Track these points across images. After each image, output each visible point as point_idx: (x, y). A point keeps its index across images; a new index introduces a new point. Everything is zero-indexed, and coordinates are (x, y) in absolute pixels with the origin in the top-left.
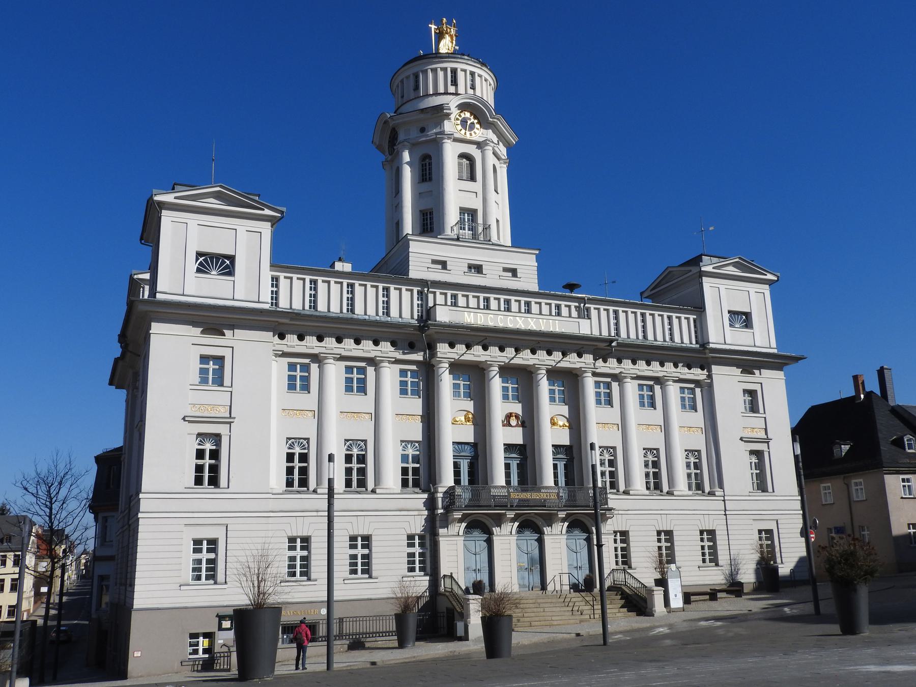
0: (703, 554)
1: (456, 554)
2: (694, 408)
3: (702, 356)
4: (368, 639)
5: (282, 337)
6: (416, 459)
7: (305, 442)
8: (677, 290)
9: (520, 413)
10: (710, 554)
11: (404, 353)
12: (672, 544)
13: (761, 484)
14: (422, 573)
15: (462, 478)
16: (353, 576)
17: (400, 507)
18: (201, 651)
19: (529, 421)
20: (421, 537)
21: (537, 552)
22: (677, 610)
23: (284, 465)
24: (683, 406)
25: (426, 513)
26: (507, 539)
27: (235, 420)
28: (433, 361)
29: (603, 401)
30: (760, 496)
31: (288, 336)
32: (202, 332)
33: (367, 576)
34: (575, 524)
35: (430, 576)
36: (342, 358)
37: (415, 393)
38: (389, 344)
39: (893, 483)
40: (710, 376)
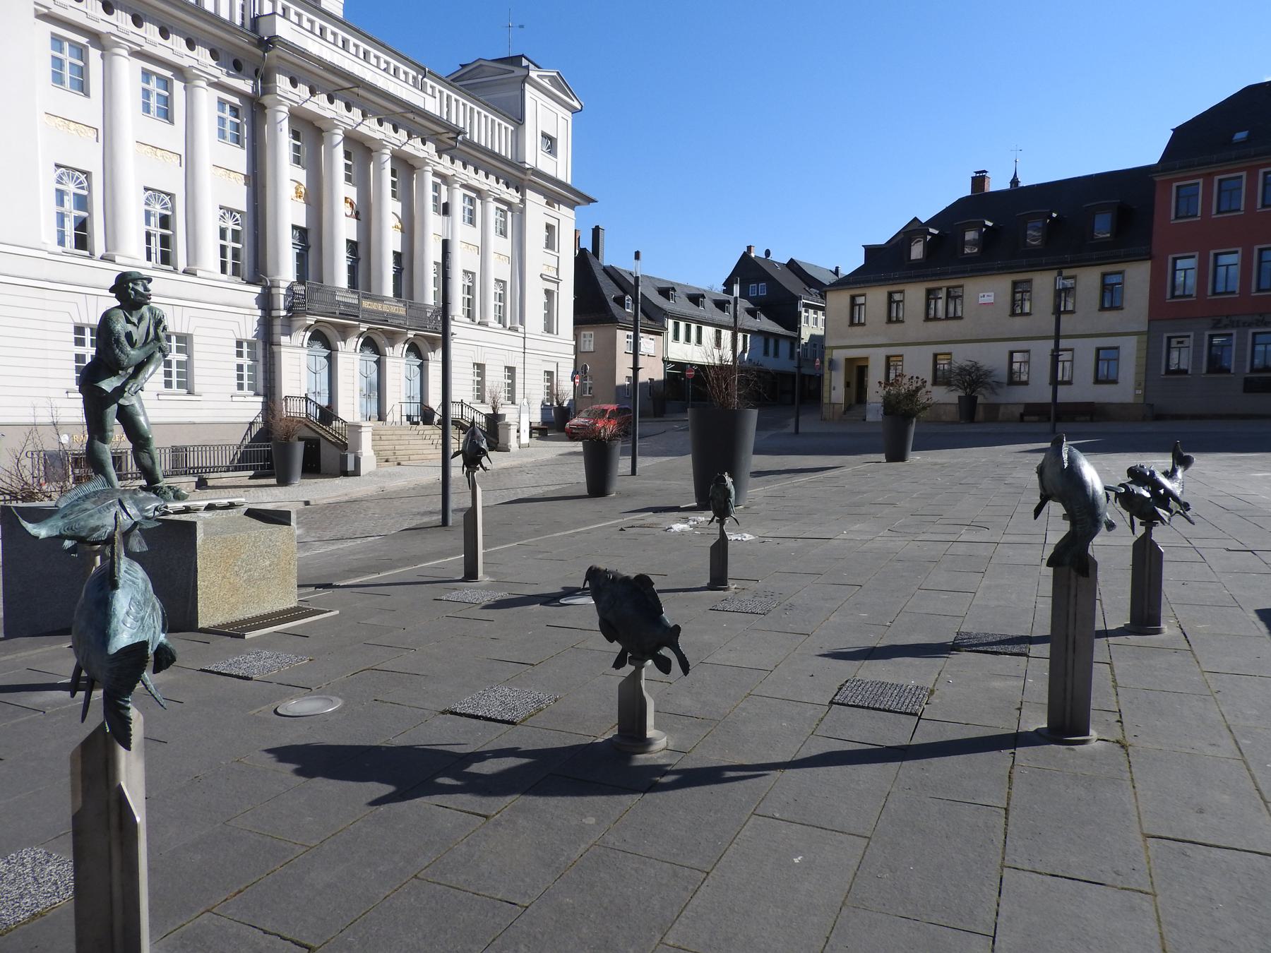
0: (240, 377)
1: (298, 369)
2: (82, 87)
3: (517, 175)
4: (212, 475)
6: (236, 236)
8: (495, 81)
11: (229, 75)
12: (483, 378)
13: (549, 328)
14: (252, 393)
15: (159, 249)
16: (168, 390)
17: (227, 301)
19: (364, 213)
20: (250, 344)
23: (54, 208)
24: (146, 108)
25: (259, 313)
26: (351, 358)
28: (267, 100)
29: (67, 81)
30: (548, 337)
31: (147, 25)
33: (185, 391)
35: (265, 396)
36: (140, 55)
38: (157, 30)
40: (523, 201)
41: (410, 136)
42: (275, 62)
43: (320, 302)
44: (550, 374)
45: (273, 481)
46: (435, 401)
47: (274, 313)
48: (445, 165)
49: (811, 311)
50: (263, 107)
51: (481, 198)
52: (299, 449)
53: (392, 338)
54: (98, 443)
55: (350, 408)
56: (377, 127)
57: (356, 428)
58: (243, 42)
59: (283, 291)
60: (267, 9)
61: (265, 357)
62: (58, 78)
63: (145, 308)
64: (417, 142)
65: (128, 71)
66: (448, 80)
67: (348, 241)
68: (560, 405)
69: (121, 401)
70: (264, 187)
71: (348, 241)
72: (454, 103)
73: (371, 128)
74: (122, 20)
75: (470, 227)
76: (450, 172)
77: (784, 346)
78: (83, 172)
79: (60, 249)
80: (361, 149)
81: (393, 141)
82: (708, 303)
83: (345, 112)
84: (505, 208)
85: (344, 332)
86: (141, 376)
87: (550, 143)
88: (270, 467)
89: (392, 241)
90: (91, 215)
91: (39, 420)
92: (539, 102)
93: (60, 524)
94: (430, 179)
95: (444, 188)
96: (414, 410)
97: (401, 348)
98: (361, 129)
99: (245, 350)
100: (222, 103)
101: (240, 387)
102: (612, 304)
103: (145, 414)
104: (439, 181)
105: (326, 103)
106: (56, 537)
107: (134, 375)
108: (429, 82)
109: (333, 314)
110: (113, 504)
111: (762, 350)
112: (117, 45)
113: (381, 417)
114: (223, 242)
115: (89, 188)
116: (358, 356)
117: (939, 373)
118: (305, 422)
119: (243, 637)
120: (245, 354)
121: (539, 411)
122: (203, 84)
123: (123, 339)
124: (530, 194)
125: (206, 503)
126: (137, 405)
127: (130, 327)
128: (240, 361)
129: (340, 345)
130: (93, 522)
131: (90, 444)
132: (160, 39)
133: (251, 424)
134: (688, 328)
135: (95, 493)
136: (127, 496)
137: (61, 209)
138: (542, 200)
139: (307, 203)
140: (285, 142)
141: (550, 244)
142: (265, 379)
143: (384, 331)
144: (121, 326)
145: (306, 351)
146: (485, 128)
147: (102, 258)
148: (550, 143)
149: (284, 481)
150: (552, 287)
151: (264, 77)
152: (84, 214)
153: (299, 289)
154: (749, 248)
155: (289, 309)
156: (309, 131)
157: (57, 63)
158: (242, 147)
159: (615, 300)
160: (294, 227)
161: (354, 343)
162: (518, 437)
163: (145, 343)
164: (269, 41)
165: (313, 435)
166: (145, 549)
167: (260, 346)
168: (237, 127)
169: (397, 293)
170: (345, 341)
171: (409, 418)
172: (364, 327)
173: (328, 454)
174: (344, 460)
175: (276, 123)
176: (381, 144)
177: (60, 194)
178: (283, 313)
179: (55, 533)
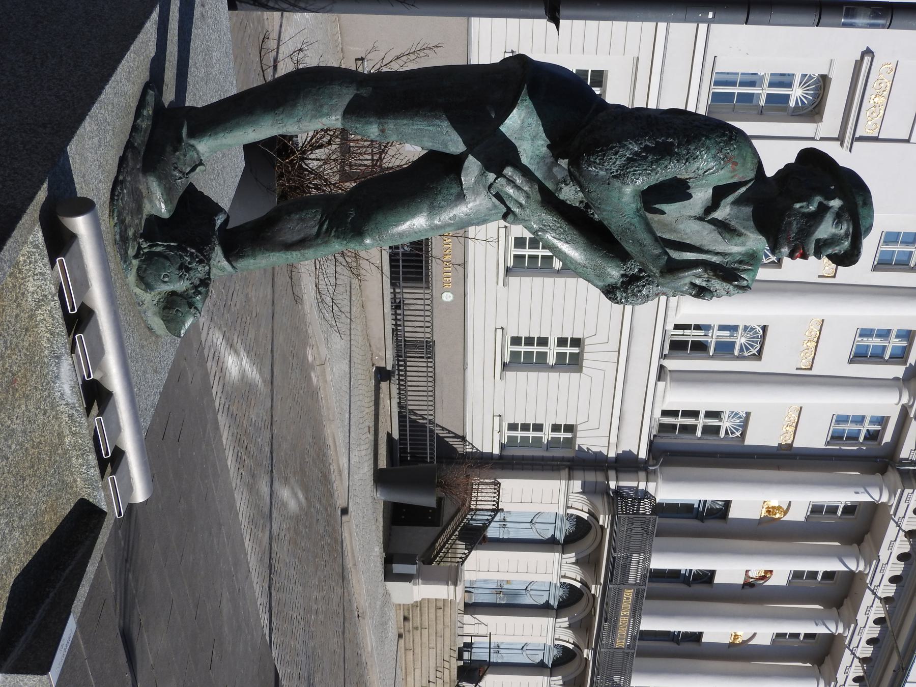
0: (525, 427)
9: (769, 583)
10: (529, 354)
14: (505, 441)
15: (690, 339)
20: (570, 442)
21: (528, 600)
24: (866, 333)
25: (612, 454)
26: (551, 571)
28: (893, 476)
29: (841, 427)
35: (501, 457)
37: (836, 437)
41: (863, 661)
45: (383, 464)
47: (612, 474)
52: (427, 501)
53: (581, 627)
55: (483, 567)
57: (453, 577)
59: (642, 486)
61: (553, 459)
63: (756, 242)
64: (879, 611)
69: (472, 166)
70: (779, 468)
80: (840, 594)
81: (856, 638)
85: (588, 563)
88: (403, 461)
89: (717, 631)
96: (480, 654)
97: (568, 638)
99: (562, 435)
100: (883, 421)
101: (513, 427)
113: (471, 608)
114: (702, 415)
116: (555, 580)
118: (463, 507)
122: (905, 400)
127: (701, 196)
128: (547, 428)
133: (463, 439)
139: (761, 521)
142: (523, 458)
143: (591, 616)
149: (381, 478)
153: (646, 507)
155: (618, 492)
158: (828, 443)
168: (853, 438)
171: (468, 646)
174: (409, 559)
175: (865, 486)
178: (613, 485)
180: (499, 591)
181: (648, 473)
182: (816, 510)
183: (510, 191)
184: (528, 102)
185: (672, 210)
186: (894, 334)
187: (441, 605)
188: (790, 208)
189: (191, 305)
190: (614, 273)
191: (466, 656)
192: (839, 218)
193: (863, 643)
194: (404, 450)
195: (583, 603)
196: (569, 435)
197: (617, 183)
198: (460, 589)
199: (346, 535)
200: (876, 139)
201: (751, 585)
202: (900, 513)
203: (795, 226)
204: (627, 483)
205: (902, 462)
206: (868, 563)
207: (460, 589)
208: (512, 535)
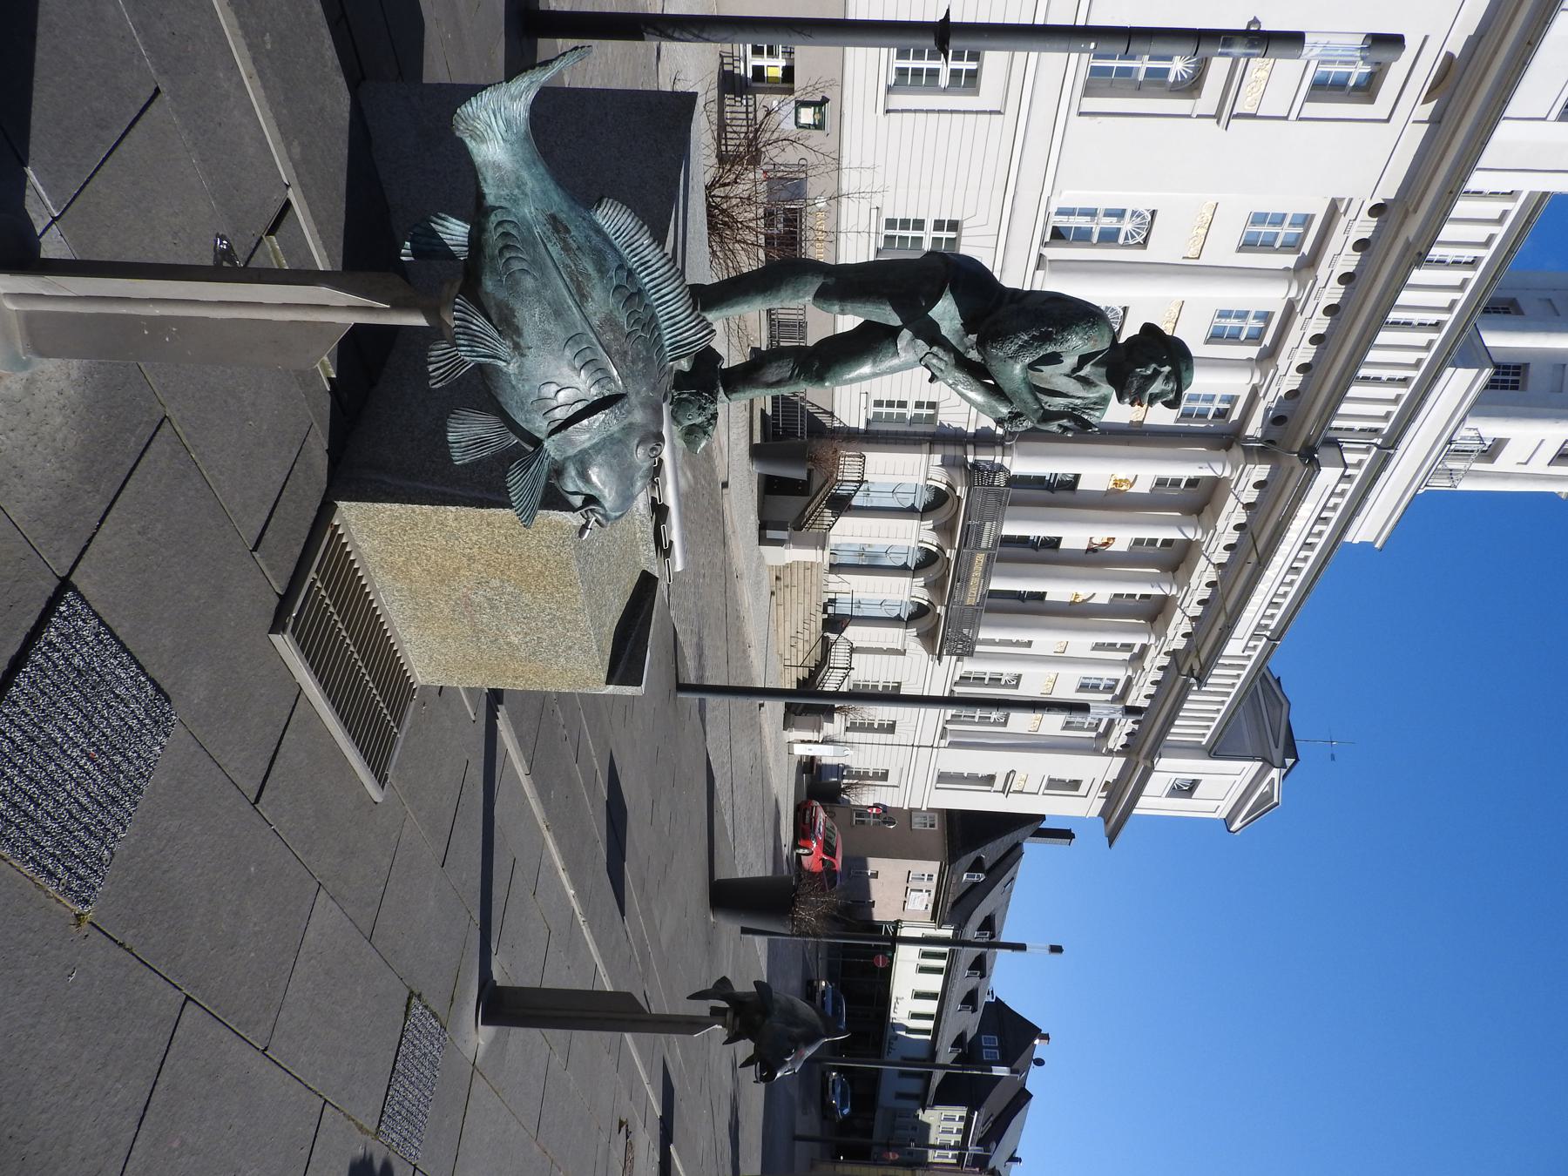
0: (890, 404)
1: (900, 473)
2: (1248, 245)
3: (1143, 750)
5: (1377, 210)
7: (1140, 239)
8: (1261, 726)
9: (1111, 549)
11: (1267, 410)
13: (944, 778)
14: (870, 416)
18: (758, 62)
20: (931, 419)
21: (888, 562)
22: (807, 127)
23: (1102, 206)
24: (1224, 314)
25: (971, 430)
26: (912, 536)
27: (1220, 129)
28: (1237, 452)
31: (1341, 289)
32: (1449, 56)
34: (920, 612)
35: (866, 432)
36: (1290, 311)
39: (933, 867)
40: (1110, 753)
41: (1193, 619)
42: (1285, 465)
43: (984, 504)
44: (884, 776)
45: (757, 440)
46: (853, 633)
47: (970, 448)
48: (1156, 660)
49: (961, 1125)
50: (1228, 447)
51: (1114, 701)
52: (799, 474)
53: (936, 586)
54: (816, 283)
55: (848, 532)
56: (1205, 580)
57: (821, 542)
58: (1309, 428)
59: (998, 460)
60: (1350, 458)
61: (915, 434)
62: (1259, 219)
63: (1106, 389)
64: (1187, 627)
65: (1273, 297)
66: (1264, 670)
67: (1059, 539)
68: (844, 790)
69: (906, 334)
70: (1128, 443)
71: (1059, 539)
72: (1235, 672)
73: (1203, 574)
74: (1333, 293)
75: (1076, 685)
76: (1147, 664)
77: (914, 1086)
78: (1146, 240)
79: (1053, 209)
80: (1176, 560)
81: (1188, 599)
82: (974, 981)
83: (1224, 543)
84: (1101, 729)
85: (945, 529)
86: (959, 376)
87: (1187, 789)
88: (775, 434)
89: (1058, 591)
90: (1094, 246)
91: (845, 174)
92: (1239, 778)
93: (528, 211)
94: (1138, 640)
95: (1127, 656)
96: (843, 609)
97: (923, 596)
98: (1202, 562)
99: (925, 411)
100: (1232, 400)
101: (878, 403)
102: (973, 856)
103: (875, 375)
104: (1136, 650)
105: (1234, 521)
106: (481, 196)
107: (963, 364)
108: (1261, 644)
109: (967, 517)
110: (602, 376)
111: (910, 1054)
112: (1302, 286)
113: (835, 568)
115: (1126, 246)
116: (913, 544)
117: (810, 58)
118: (830, 479)
119: (277, 626)
120: (919, 411)
121: (835, 761)
122: (1256, 380)
123: (1050, 349)
124: (1119, 762)
125: (671, 500)
126: (895, 362)
127: (1070, 361)
128: (911, 405)
129: (929, 524)
130: (531, 318)
131: (817, 268)
132: (1310, 333)
133: (832, 414)
134: (941, 956)
135: (651, 324)
136: (638, 416)
137: (1101, 213)
138: (1112, 776)
139: (1108, 492)
140: (1185, 471)
141: (1054, 784)
142: (887, 433)
143: (944, 577)
144: (1075, 345)
145: (921, 483)
146: (1203, 711)
147: (1041, 255)
148: (1187, 789)
149: (756, 453)
150: (999, 784)
151: (1266, 450)
152: (1095, 239)
153: (1000, 480)
154: (1046, 1037)
155: (975, 465)
156: (1200, 500)
157: (1279, 220)
158: (1178, 421)
159: (979, 860)
160: (1077, 477)
161: (931, 540)
162: (803, 742)
163: (1035, 389)
164: (1312, 459)
165: (815, 488)
166: (459, 458)
167: (929, 429)
168: (1202, 415)
169: (994, 594)
170: (934, 529)
171: (833, 601)
172: (950, 554)
173: (790, 505)
174: (781, 526)
175: (1209, 461)
176: (1184, 583)
177: (1120, 214)
178: (970, 459)
179: (491, 194)
180: (862, 553)
181: (1004, 447)
182: (1161, 482)
183: (935, 361)
184: (950, 296)
185: (1048, 370)
186: (1252, 315)
187: (809, 567)
188: (1133, 370)
189: (705, 433)
190: (1004, 410)
191: (830, 610)
192: (1167, 379)
193: (1194, 603)
194: (776, 426)
195: (938, 565)
196: (931, 412)
197: (1011, 362)
198: (827, 552)
199: (726, 506)
200: (1254, 116)
201: (1095, 550)
202: (1211, 549)
203: (1135, 384)
204: (984, 457)
205: (1246, 439)
206: (1180, 588)
207: (827, 552)
208: (875, 504)
